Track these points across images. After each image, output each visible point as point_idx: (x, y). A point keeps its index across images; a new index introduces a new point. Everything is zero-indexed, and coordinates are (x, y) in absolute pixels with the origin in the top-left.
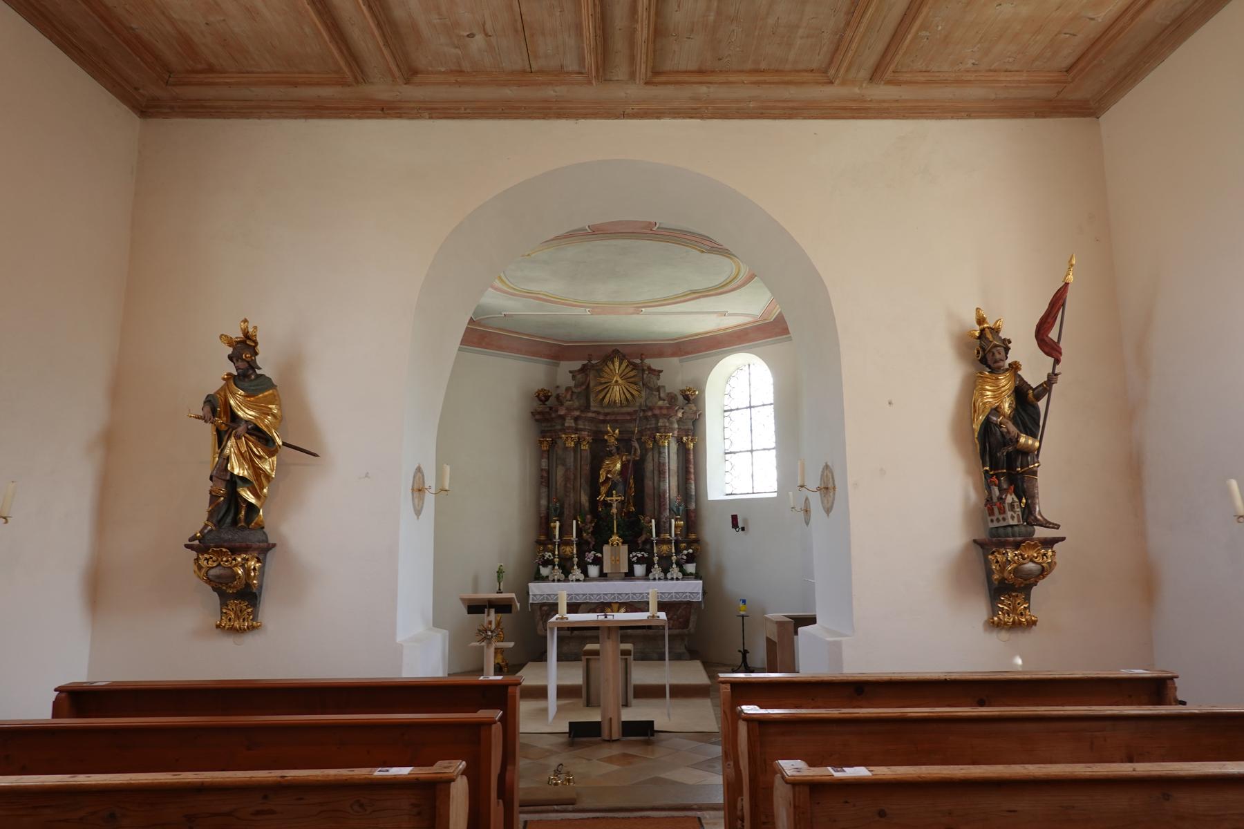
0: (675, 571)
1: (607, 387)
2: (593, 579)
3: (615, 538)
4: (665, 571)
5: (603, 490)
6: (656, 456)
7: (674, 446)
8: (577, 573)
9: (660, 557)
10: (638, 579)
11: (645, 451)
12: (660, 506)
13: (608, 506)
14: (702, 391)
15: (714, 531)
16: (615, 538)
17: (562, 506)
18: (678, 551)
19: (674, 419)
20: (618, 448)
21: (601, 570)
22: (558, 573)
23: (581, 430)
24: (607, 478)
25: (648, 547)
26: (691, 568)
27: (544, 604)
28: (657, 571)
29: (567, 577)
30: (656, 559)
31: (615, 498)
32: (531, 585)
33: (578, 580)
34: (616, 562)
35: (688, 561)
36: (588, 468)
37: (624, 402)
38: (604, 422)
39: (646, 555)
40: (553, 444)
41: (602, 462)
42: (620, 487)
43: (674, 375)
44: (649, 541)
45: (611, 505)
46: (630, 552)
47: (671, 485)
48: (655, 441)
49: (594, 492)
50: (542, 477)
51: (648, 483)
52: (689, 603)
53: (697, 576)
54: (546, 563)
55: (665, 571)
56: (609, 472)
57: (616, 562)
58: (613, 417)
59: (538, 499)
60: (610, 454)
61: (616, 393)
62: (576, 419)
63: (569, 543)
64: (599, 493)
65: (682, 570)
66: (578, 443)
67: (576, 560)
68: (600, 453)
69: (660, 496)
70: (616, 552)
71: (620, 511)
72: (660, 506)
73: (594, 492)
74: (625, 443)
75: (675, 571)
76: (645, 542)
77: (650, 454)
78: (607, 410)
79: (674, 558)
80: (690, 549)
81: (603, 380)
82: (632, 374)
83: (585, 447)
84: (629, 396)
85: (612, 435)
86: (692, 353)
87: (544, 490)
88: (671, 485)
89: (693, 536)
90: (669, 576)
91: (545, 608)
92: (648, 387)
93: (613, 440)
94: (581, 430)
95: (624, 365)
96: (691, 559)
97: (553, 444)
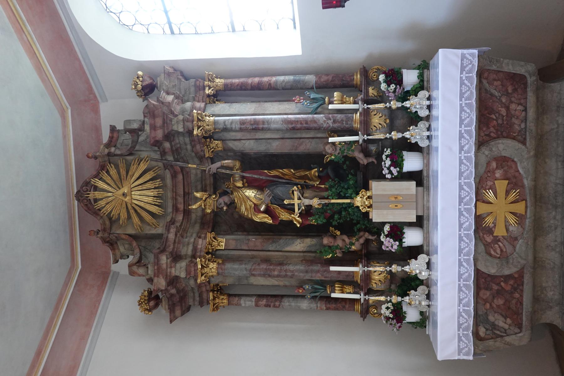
0: (416, 104)
1: (135, 210)
2: (427, 237)
3: (358, 201)
4: (414, 119)
5: (284, 216)
6: (233, 135)
7: (220, 107)
8: (416, 267)
9: (391, 128)
10: (427, 164)
11: (227, 153)
12: (308, 129)
13: (308, 212)
14: (141, 65)
15: (351, 39)
16: (358, 201)
17: (310, 281)
18: (381, 98)
19: (177, 108)
20: (225, 193)
21: (410, 225)
22: (416, 297)
23: (195, 249)
24: (267, 211)
25: (373, 148)
26: (410, 78)
27: (476, 335)
28: (415, 134)
29: (421, 282)
30: (395, 135)
31: (298, 201)
32: (440, 357)
33: (429, 265)
34: (396, 201)
35: (400, 82)
36: (253, 238)
37: (158, 183)
38: (187, 213)
39: (390, 151)
40: (219, 290)
41: (241, 216)
42: (280, 191)
43: (120, 109)
44: (364, 148)
45: (309, 207)
46: (382, 177)
47: (276, 113)
48: (209, 137)
49: (284, 229)
50: (267, 306)
51: (276, 147)
52: (480, 74)
53: (424, 67)
54: (398, 314)
55: (414, 119)
56: (256, 208)
57: (396, 201)
58: (180, 200)
59: (299, 310)
60: (232, 205)
61: (143, 197)
62: (176, 258)
63: (367, 276)
64: (291, 222)
65: (415, 91)
66: (213, 254)
67: (395, 268)
68: (227, 220)
69: (294, 129)
70: (385, 202)
71: (318, 192)
72: (308, 129)
73: (284, 229)
74: (218, 184)
75: (416, 104)
76: (367, 154)
77: (231, 144)
78: (170, 210)
79: (395, 104)
80: (386, 83)
81: (124, 215)
82: (113, 172)
83: (222, 243)
84: (148, 177)
85: (203, 202)
86: (87, 82)
87: (286, 303)
88: (276, 113)
89: (358, 78)
90: (423, 113)
91: (482, 331)
92: (133, 147)
93: (210, 201)
94: (195, 249)
95: (101, 184)
96: (394, 77)
97: (219, 290)
